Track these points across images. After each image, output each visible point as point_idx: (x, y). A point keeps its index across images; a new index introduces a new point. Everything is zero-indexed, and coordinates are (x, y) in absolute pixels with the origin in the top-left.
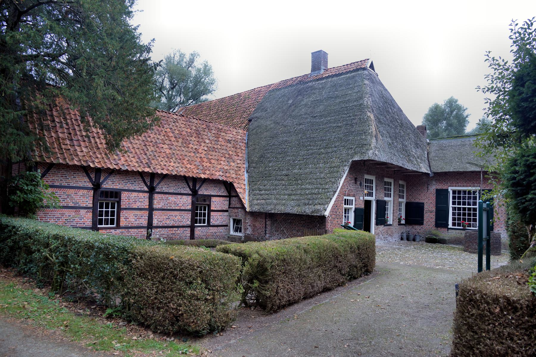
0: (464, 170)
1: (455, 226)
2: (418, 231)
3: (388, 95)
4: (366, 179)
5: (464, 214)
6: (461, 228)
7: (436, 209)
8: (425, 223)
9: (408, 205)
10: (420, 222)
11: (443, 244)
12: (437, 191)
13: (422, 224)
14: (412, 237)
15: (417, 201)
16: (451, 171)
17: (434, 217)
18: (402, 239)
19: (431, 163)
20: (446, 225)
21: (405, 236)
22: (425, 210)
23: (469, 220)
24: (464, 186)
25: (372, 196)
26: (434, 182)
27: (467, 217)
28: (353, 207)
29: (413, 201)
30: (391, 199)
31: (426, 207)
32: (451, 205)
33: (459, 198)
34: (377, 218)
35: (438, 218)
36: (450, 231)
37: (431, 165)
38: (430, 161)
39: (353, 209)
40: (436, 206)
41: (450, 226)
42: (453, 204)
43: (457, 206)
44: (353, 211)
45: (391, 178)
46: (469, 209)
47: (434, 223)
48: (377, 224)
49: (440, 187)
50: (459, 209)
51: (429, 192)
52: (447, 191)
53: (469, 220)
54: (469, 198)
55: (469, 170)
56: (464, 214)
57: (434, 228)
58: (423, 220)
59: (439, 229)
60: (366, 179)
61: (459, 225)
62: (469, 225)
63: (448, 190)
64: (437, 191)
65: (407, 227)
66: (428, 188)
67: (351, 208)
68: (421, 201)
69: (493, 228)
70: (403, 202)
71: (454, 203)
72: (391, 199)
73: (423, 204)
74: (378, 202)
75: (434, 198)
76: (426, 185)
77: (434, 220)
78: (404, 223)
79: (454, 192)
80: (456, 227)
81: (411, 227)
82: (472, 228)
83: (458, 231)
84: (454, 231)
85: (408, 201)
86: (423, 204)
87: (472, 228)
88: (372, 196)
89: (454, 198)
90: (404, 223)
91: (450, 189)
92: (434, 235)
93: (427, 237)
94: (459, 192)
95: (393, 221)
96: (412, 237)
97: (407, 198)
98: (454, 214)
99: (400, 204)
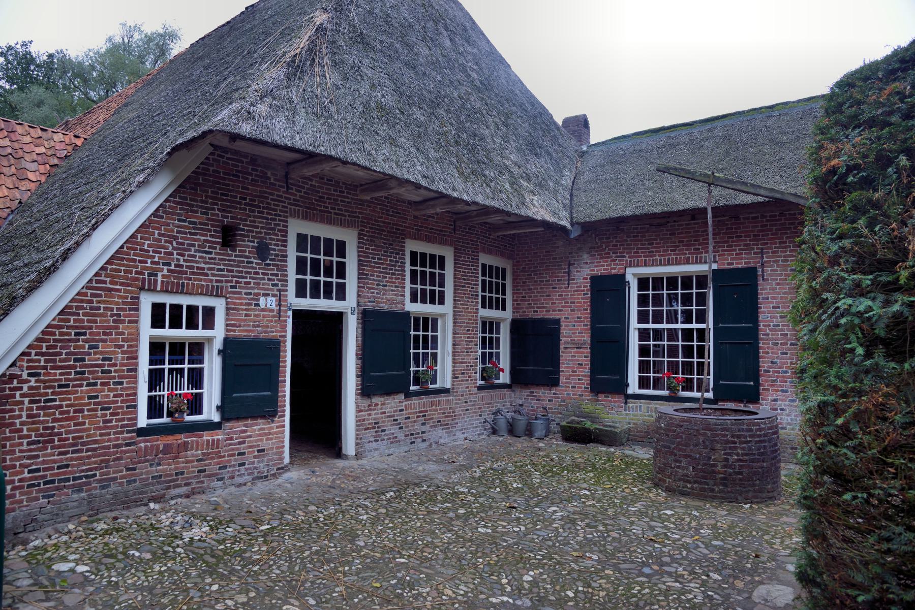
0: (665, 209)
1: (648, 387)
2: (546, 403)
3: (459, 14)
4: (484, 266)
5: (673, 351)
6: (665, 393)
7: (592, 337)
8: (562, 379)
9: (517, 326)
10: (551, 380)
11: (611, 445)
12: (595, 280)
13: (555, 383)
14: (521, 425)
15: (541, 314)
16: (627, 213)
17: (587, 362)
18: (494, 432)
19: (575, 198)
20: (619, 388)
21: (502, 423)
22: (563, 340)
23: (688, 368)
24: (668, 263)
25: (504, 309)
26: (585, 256)
27: (680, 359)
28: (218, 333)
29: (531, 315)
30: (447, 309)
31: (565, 332)
32: (634, 325)
33: (658, 300)
34: (363, 373)
35: (597, 366)
36: (632, 403)
37: (574, 204)
38: (575, 193)
39: (218, 344)
40: (592, 329)
41: (634, 387)
42: (640, 321)
43: (651, 326)
44: (215, 352)
45: (509, 258)
46: (688, 334)
47: (586, 381)
48: (366, 391)
49: (602, 268)
50: (658, 334)
51: (573, 287)
52: (621, 280)
53: (688, 368)
54: (672, 299)
55: (680, 207)
56: (673, 351)
57: (588, 396)
58: (557, 371)
59: (601, 397)
60: (484, 266)
61: (657, 384)
62: (688, 386)
63: (623, 276)
64: (595, 280)
65: (518, 393)
66: (569, 275)
67: (210, 340)
68: (552, 315)
69: (758, 394)
70: (504, 320)
71: (643, 317)
72: (447, 309)
73: (557, 322)
74: (367, 317)
75: (587, 306)
76: (565, 266)
77: (587, 371)
78: (508, 381)
79: (643, 283)
80: (651, 392)
81: (526, 392)
82: (695, 394)
83: (654, 404)
84: (643, 404)
85: (518, 316)
86: (557, 322)
87: (695, 394)
88: (504, 309)
89: (643, 300)
90: (508, 381)
91: (632, 275)
92: (587, 416)
93: (564, 423)
94: (658, 281)
95: (455, 377)
96: (521, 425)
97: (516, 309)
98: (643, 351)
99: (490, 326)
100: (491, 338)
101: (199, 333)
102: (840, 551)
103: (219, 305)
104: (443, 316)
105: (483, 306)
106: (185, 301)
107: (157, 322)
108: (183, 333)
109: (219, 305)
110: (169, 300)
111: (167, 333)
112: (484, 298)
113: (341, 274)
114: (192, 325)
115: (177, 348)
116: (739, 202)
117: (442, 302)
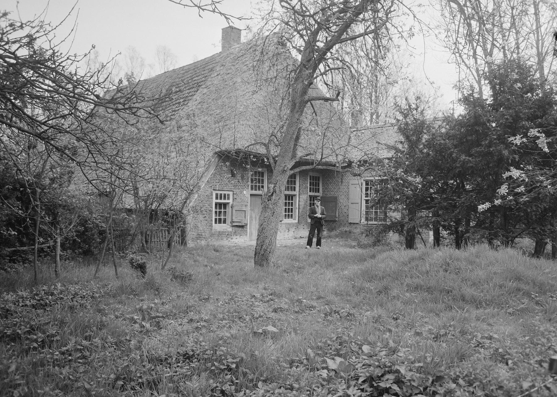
25: (318, 192)
67: (228, 203)
97: (324, 192)
100: (289, 200)
101: (226, 201)
102: (222, 56)
103: (231, 193)
104: (295, 195)
105: (310, 191)
106: (223, 193)
107: (217, 198)
108: (223, 201)
109: (231, 193)
110: (219, 192)
111: (219, 201)
112: (310, 188)
113: (263, 183)
114: (225, 198)
115: (220, 204)
116: (545, 69)
117: (295, 190)
